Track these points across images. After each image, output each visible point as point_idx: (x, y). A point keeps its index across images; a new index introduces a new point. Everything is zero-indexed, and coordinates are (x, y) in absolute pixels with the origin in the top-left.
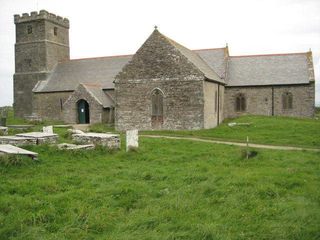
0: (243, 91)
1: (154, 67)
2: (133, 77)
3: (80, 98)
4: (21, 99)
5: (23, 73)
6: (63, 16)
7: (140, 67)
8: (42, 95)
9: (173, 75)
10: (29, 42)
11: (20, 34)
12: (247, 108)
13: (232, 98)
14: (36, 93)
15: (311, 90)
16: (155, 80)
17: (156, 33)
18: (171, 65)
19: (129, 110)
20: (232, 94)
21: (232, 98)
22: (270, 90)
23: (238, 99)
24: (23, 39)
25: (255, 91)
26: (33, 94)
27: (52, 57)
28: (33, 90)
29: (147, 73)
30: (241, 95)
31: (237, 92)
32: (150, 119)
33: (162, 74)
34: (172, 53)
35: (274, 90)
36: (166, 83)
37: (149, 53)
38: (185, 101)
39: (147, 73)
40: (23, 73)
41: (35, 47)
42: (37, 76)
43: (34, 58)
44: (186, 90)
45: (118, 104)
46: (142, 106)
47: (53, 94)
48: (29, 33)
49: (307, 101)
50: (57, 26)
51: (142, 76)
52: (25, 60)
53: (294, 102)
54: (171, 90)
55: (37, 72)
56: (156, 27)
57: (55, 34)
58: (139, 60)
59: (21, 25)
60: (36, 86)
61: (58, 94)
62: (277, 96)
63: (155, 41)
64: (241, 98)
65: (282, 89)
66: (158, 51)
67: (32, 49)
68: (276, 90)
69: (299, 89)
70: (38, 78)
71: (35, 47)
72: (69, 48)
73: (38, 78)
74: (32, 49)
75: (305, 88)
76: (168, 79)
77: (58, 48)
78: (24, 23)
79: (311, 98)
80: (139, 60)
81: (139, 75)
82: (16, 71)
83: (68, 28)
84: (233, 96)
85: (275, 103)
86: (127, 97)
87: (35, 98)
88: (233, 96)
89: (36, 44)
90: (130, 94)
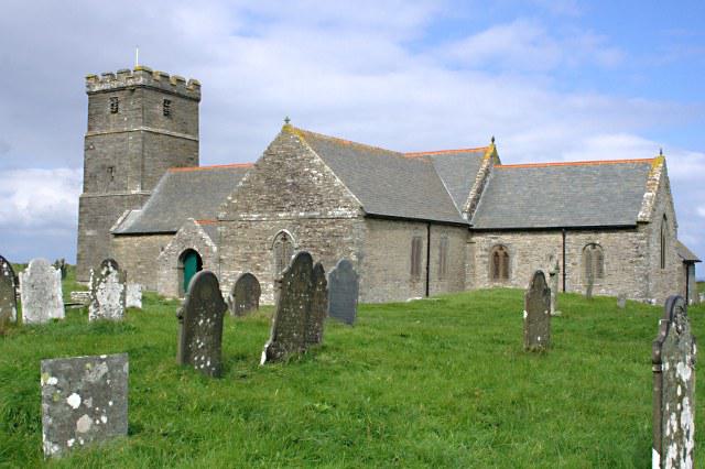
0: (506, 239)
1: (282, 193)
2: (248, 209)
3: (187, 247)
4: (92, 247)
5: (98, 194)
6: (187, 76)
7: (260, 191)
8: (129, 238)
9: (311, 208)
10: (112, 130)
11: (97, 113)
12: (513, 276)
13: (484, 253)
14: (117, 235)
15: (642, 239)
16: (282, 215)
17: (286, 130)
18: (309, 190)
19: (239, 269)
20: (485, 246)
21: (484, 253)
22: (559, 237)
23: (496, 254)
24: (101, 124)
25: (528, 239)
26: (112, 236)
27: (155, 161)
28: (112, 229)
29: (270, 202)
30: (501, 247)
31: (494, 241)
32: (271, 286)
33: (294, 206)
34: (311, 166)
35: (567, 237)
36: (299, 221)
37: (274, 167)
38: (328, 254)
39: (270, 202)
40: (98, 194)
41: (123, 141)
42: (123, 201)
43: (120, 164)
44: (330, 235)
45: (223, 257)
46: (259, 262)
47: (149, 238)
48: (113, 112)
49: (632, 262)
50: (169, 98)
51: (262, 207)
52: (103, 167)
53: (607, 263)
54: (306, 235)
55: (124, 192)
56: (287, 121)
57: (167, 114)
58: (258, 179)
59: (98, 95)
60: (119, 221)
61: (158, 237)
62: (573, 251)
63: (286, 145)
64: (501, 253)
65: (582, 237)
66: (288, 163)
67: (117, 145)
68: (570, 237)
69: (616, 237)
70: (126, 203)
71: (123, 141)
72: (197, 142)
73: (126, 203)
74: (117, 145)
75: (630, 234)
76: (302, 214)
77: (170, 143)
78: (105, 91)
79: (641, 256)
80: (258, 179)
81: (258, 206)
82: (85, 190)
83: (198, 100)
84: (486, 250)
85: (569, 265)
86: (235, 243)
87: (116, 245)
88: (486, 250)
89: (124, 135)
90: (241, 239)
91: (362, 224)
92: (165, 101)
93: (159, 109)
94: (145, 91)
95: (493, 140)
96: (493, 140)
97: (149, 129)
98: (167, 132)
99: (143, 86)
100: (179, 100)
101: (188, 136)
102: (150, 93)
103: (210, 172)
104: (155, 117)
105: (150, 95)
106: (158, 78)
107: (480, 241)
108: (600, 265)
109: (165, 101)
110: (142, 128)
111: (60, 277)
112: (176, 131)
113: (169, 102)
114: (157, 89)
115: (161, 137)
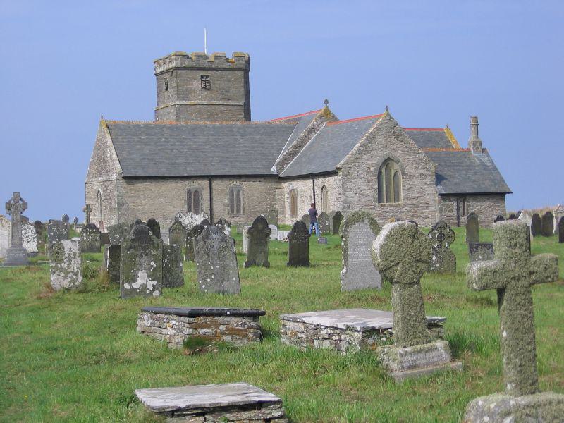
35: (316, 181)
57: (206, 87)
91: (122, 181)
92: (202, 77)
93: (196, 84)
94: (179, 72)
95: (326, 102)
96: (326, 102)
97: (185, 102)
98: (205, 102)
99: (177, 68)
100: (219, 73)
101: (231, 102)
102: (184, 72)
103: (256, 126)
104: (192, 91)
105: (191, 74)
106: (212, 59)
107: (285, 185)
108: (231, 201)
109: (202, 77)
110: (177, 102)
111: (468, 252)
112: (217, 99)
113: (207, 77)
114: (192, 68)
115: (198, 107)
